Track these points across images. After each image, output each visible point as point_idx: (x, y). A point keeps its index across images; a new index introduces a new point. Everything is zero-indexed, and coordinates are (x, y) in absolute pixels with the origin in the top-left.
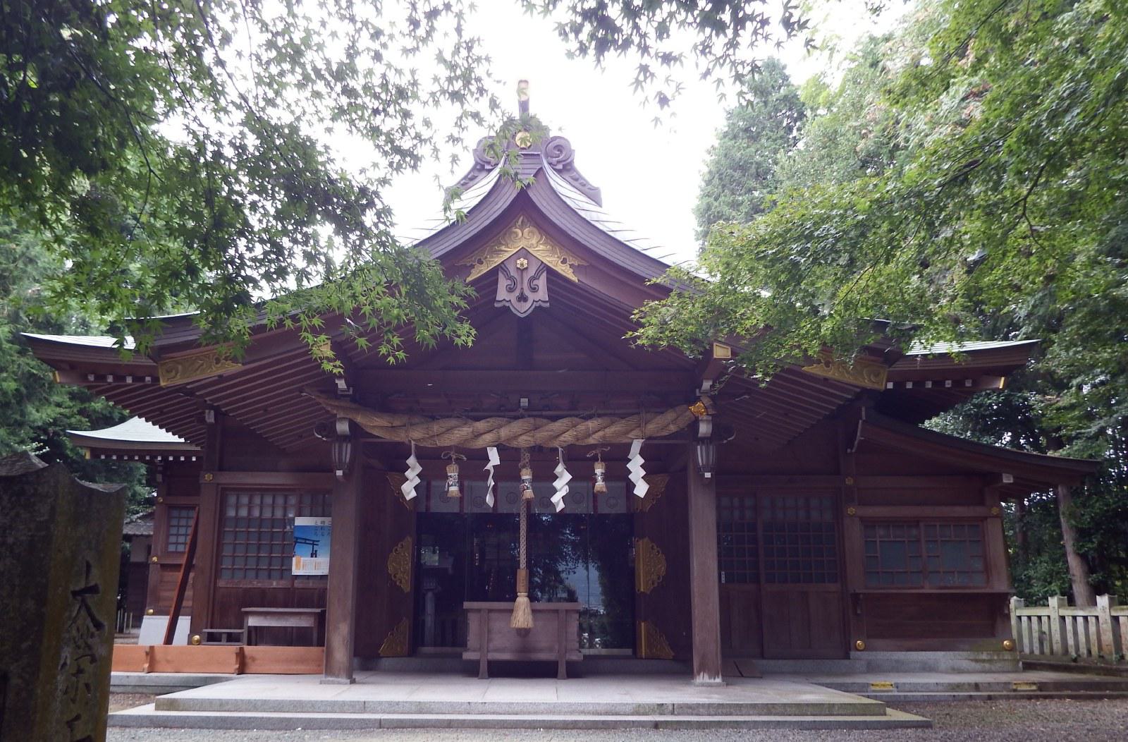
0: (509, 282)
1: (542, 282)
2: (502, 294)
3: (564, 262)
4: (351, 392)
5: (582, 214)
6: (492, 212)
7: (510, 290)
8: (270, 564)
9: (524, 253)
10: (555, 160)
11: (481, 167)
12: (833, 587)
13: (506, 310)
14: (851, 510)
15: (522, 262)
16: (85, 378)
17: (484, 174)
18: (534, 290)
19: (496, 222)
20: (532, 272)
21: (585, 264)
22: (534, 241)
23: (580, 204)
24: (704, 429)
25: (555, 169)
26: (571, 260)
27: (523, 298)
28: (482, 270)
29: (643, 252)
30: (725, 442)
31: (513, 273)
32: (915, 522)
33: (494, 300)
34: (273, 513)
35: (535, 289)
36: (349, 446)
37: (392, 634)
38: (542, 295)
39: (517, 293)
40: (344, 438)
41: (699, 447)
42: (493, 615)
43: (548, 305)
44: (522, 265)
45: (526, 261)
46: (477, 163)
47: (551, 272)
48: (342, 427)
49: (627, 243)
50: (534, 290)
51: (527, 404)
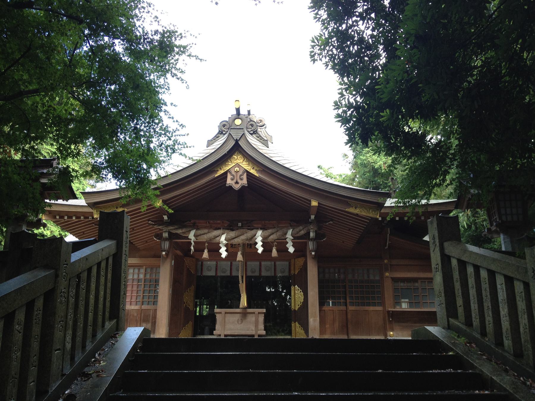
0: (232, 177)
1: (245, 177)
2: (229, 181)
3: (253, 168)
4: (169, 221)
5: (261, 151)
6: (225, 150)
7: (232, 179)
8: (131, 299)
9: (238, 165)
10: (250, 130)
11: (221, 133)
12: (380, 308)
13: (231, 187)
14: (387, 274)
15: (237, 169)
16: (55, 217)
17: (222, 135)
18: (241, 179)
19: (225, 155)
20: (241, 173)
21: (261, 169)
22: (242, 161)
23: (259, 147)
24: (312, 235)
25: (249, 133)
26: (256, 168)
27: (237, 183)
28: (221, 172)
29: (283, 165)
30: (322, 241)
31: (233, 173)
32: (415, 280)
33: (226, 184)
34: (133, 276)
35: (242, 179)
36: (168, 242)
37: (185, 329)
38: (245, 182)
39: (235, 181)
40: (166, 239)
41: (310, 242)
42: (227, 315)
43: (247, 185)
44: (237, 170)
45: (238, 169)
46: (220, 131)
47: (247, 172)
48: (166, 235)
49: (277, 162)
50: (241, 179)
51: (241, 225)
